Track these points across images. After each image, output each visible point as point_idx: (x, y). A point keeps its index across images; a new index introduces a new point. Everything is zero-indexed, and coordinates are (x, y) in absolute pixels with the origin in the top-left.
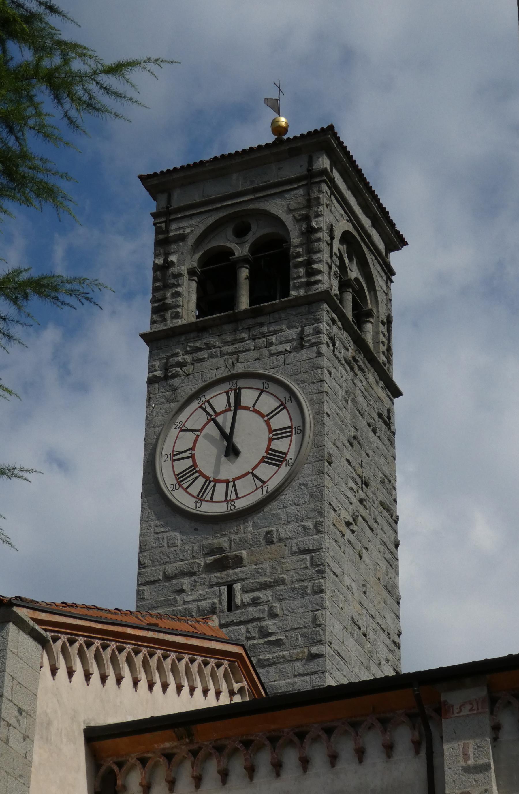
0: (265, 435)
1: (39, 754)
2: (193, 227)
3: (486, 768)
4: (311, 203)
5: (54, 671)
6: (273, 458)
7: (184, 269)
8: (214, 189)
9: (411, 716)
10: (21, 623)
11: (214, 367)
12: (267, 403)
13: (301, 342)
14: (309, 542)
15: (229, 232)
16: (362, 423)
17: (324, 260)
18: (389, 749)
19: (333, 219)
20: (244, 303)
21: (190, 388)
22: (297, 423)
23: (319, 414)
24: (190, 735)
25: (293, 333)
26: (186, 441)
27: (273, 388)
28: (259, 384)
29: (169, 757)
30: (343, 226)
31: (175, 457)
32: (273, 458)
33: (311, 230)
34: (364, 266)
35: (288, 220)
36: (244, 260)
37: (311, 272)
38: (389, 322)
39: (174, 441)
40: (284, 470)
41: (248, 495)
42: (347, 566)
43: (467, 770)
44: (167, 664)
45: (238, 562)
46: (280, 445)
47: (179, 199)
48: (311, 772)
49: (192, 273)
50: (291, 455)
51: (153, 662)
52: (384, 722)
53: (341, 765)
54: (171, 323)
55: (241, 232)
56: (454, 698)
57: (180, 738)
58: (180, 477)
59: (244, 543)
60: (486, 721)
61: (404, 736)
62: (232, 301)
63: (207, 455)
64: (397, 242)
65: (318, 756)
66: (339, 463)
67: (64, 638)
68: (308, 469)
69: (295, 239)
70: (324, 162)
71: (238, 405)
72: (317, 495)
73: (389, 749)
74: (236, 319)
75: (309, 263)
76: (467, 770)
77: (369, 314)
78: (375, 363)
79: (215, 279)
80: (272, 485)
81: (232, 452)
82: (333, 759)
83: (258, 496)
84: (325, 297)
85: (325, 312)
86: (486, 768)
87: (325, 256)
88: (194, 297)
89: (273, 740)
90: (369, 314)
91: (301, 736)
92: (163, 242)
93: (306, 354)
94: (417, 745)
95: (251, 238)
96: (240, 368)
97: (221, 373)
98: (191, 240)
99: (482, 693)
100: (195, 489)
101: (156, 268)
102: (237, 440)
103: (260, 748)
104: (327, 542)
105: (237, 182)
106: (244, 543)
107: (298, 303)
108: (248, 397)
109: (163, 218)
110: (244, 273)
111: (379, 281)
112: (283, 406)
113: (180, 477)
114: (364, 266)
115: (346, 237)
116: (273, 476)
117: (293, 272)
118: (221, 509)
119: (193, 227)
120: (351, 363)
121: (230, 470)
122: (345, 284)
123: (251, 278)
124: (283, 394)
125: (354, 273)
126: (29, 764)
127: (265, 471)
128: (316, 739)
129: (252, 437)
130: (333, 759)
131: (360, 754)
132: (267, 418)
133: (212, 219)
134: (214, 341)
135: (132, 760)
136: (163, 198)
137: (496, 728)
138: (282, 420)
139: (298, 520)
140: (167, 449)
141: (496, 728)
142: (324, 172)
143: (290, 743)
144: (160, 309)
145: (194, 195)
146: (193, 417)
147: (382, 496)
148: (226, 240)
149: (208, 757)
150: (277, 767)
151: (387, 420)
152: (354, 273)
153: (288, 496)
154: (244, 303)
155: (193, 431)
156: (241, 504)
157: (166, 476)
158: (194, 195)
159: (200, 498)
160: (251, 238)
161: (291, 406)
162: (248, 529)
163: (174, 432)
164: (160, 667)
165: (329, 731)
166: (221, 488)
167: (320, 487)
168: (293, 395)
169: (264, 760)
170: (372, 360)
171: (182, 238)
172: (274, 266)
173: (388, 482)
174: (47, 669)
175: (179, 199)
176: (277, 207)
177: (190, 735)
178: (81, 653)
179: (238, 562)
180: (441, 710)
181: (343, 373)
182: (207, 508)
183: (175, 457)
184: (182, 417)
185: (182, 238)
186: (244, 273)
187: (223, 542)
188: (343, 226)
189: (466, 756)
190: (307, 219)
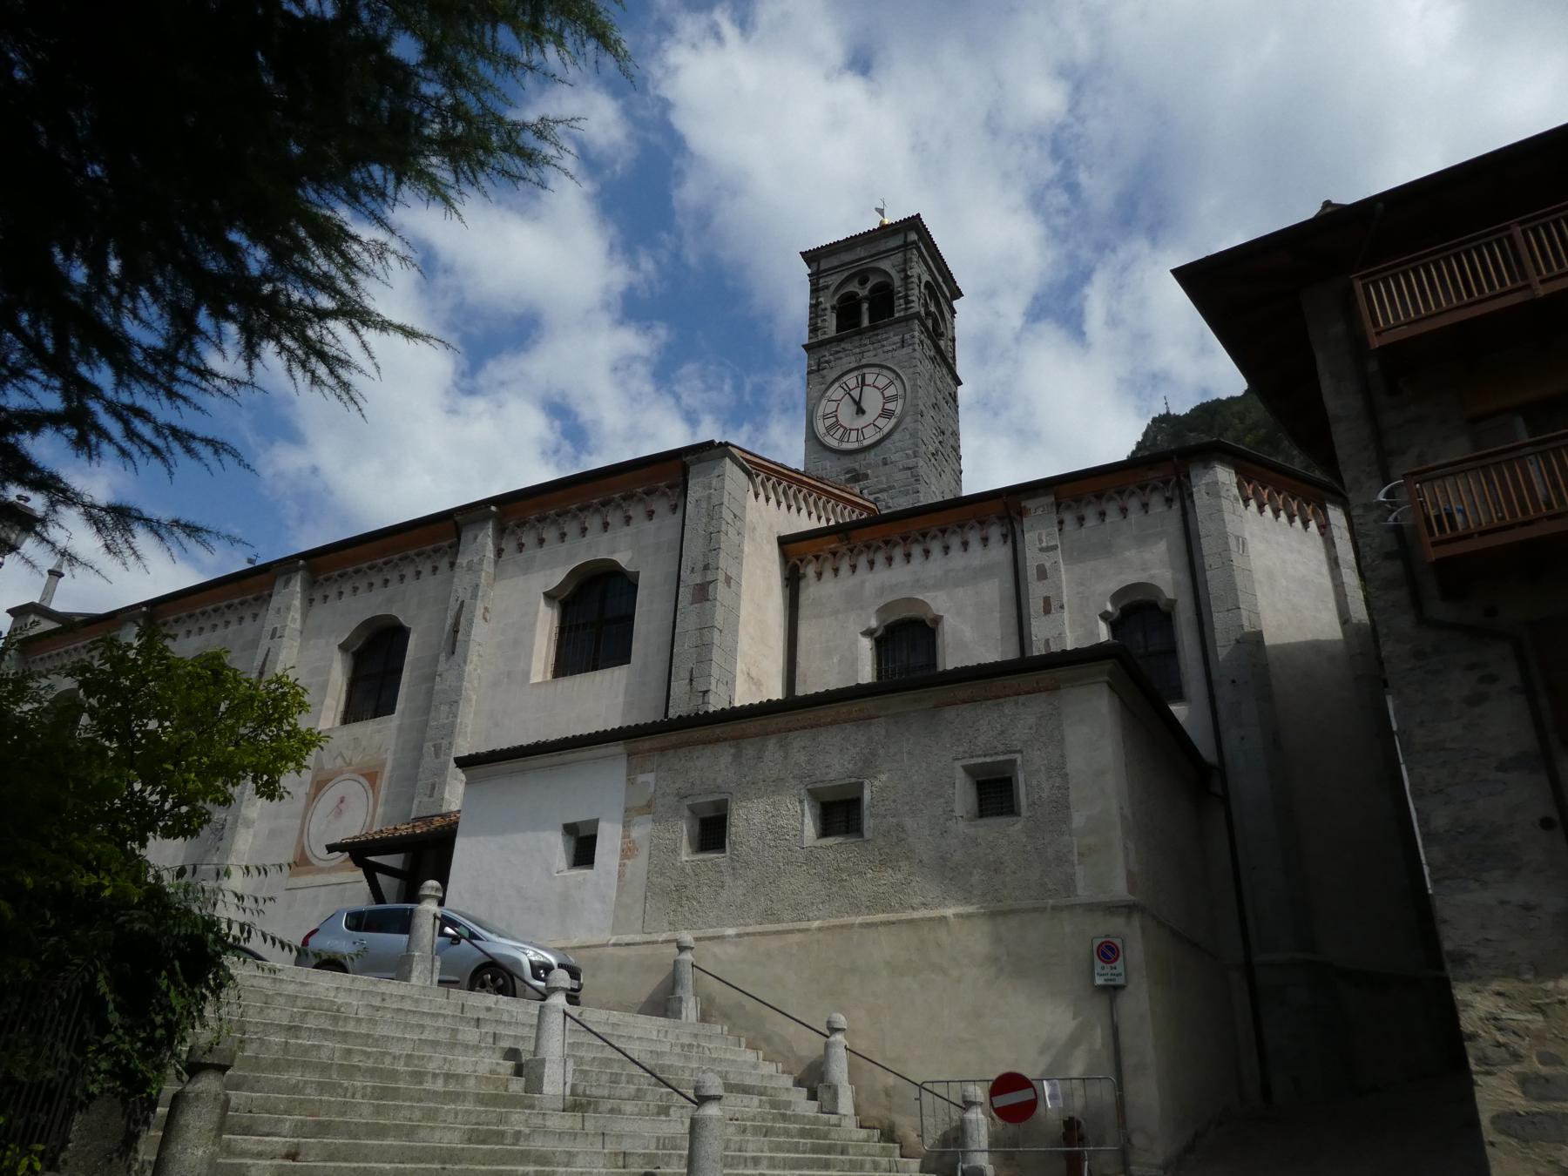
0: (881, 400)
1: (747, 548)
2: (834, 280)
3: (1055, 548)
4: (906, 261)
5: (757, 495)
6: (886, 414)
7: (828, 306)
8: (846, 257)
9: (1000, 518)
10: (734, 459)
11: (849, 362)
12: (882, 381)
13: (903, 343)
14: (910, 462)
15: (856, 282)
16: (940, 397)
17: (914, 294)
18: (985, 541)
19: (918, 270)
20: (866, 322)
21: (835, 376)
22: (901, 392)
23: (914, 386)
24: (848, 539)
25: (897, 339)
26: (831, 407)
27: (885, 372)
28: (877, 370)
29: (834, 554)
30: (926, 277)
31: (825, 417)
32: (886, 414)
33: (907, 277)
34: (938, 305)
35: (893, 272)
36: (866, 298)
37: (908, 302)
38: (953, 340)
39: (826, 407)
40: (893, 421)
41: (871, 437)
42: (933, 480)
43: (1041, 550)
44: (829, 506)
45: (866, 477)
46: (890, 406)
47: (824, 265)
48: (931, 558)
49: (833, 308)
50: (898, 412)
51: (821, 504)
52: (982, 523)
53: (952, 553)
54: (821, 338)
55: (863, 282)
56: (1030, 504)
57: (841, 541)
58: (828, 429)
59: (869, 466)
60: (1055, 518)
61: (995, 533)
62: (858, 324)
63: (846, 414)
64: (957, 294)
65: (936, 547)
66: (928, 417)
67: (763, 475)
68: (908, 419)
69: (897, 282)
70: (913, 237)
71: (863, 383)
72: (914, 435)
73: (985, 541)
74: (861, 332)
75: (906, 296)
76: (1041, 550)
77: (942, 335)
78: (945, 360)
79: (847, 312)
80: (886, 430)
81: (861, 411)
82: (946, 549)
83: (878, 437)
84: (917, 316)
85: (916, 324)
86: (1055, 548)
87: (916, 292)
88: (834, 322)
89: (905, 539)
90: (942, 335)
91: (924, 536)
92: (815, 290)
93: (905, 351)
94: (1005, 536)
95: (869, 285)
96: (864, 362)
97: (853, 365)
98: (832, 289)
99: (1052, 499)
100: (838, 435)
101: (811, 306)
102: (864, 405)
103: (896, 545)
104: (921, 463)
105: (860, 252)
106: (869, 466)
107: (899, 321)
108: (869, 379)
109: (815, 277)
110: (865, 306)
111: (948, 316)
112: (892, 383)
113: (828, 429)
114: (938, 305)
115: (927, 283)
116: (886, 425)
117: (896, 303)
118: (855, 446)
119: (834, 280)
120: (933, 359)
121: (861, 422)
122: (928, 314)
123: (870, 309)
124: (891, 376)
125: (933, 309)
126: (742, 551)
127: (881, 422)
128: (934, 537)
129: (873, 401)
130: (946, 549)
131: (965, 545)
132: (882, 390)
133: (846, 274)
134: (848, 346)
135: (810, 557)
136: (815, 266)
137: (1061, 522)
138: (891, 391)
139: (903, 450)
140: (820, 413)
141: (1061, 522)
142: (914, 242)
143: (917, 541)
144: (814, 329)
145: (835, 261)
146: (836, 392)
147: (952, 442)
148: (853, 287)
149: (861, 552)
150: (908, 557)
151: (954, 397)
152: (933, 309)
153: (896, 436)
154: (866, 322)
155: (836, 402)
156: (866, 443)
157: (820, 428)
158: (835, 261)
159: (841, 440)
160: (869, 285)
161: (897, 383)
162: (871, 456)
163: (824, 402)
164: (825, 508)
165: (943, 532)
166: (854, 434)
167: (916, 430)
168: (898, 375)
169: (898, 553)
170: (945, 360)
171: (827, 287)
172: (883, 300)
173: (955, 434)
174: (751, 493)
175: (824, 265)
176: (885, 265)
177: (848, 539)
178: (774, 488)
179: (866, 477)
180: (1022, 513)
181: (928, 364)
182: (845, 446)
183: (825, 417)
184: (829, 393)
185: (827, 287)
186: (865, 306)
187: (856, 466)
188: (926, 277)
189: (1040, 541)
190: (904, 270)
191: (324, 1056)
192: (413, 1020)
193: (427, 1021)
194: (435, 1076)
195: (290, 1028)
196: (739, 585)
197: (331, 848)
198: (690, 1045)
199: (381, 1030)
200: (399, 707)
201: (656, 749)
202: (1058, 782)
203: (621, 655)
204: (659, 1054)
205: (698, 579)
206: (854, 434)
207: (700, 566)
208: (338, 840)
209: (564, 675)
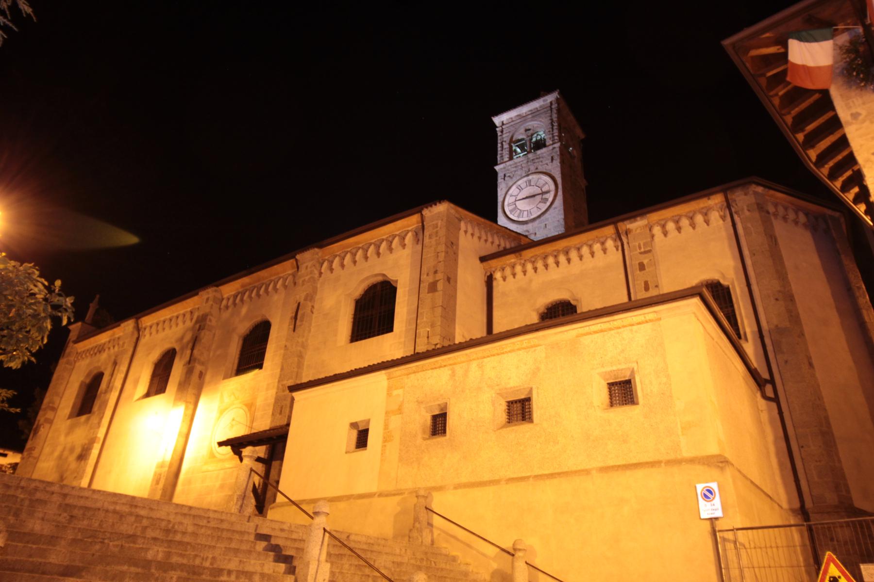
43: (641, 253)
76: (641, 253)
80: (544, 210)
83: (539, 213)
100: (516, 215)
166: (525, 213)
182: (521, 219)
189: (640, 248)
191: (150, 555)
192: (225, 535)
193: (237, 536)
194: (229, 572)
195: (129, 536)
196: (456, 282)
197: (221, 444)
198: (422, 559)
199: (202, 541)
200: (267, 363)
201: (405, 375)
202: (664, 380)
203: (388, 327)
204: (400, 564)
205: (431, 279)
206: (525, 213)
207: (432, 271)
208: (224, 439)
209: (357, 340)
